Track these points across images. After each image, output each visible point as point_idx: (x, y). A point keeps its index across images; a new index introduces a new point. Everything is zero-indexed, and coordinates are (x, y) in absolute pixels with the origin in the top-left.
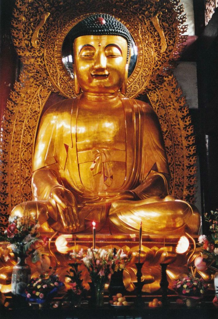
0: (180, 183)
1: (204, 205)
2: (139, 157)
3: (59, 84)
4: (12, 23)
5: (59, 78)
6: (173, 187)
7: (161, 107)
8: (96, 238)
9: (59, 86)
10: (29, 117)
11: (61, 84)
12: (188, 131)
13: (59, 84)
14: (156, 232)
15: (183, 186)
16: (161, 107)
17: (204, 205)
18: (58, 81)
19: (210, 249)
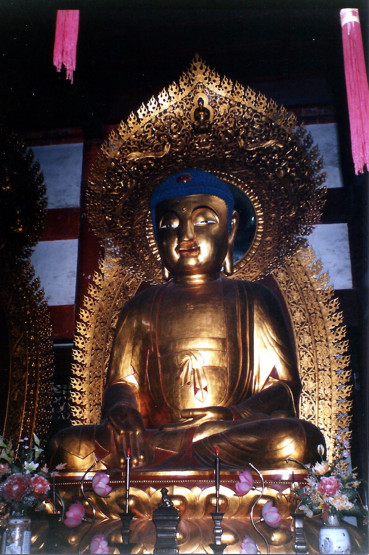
0: (327, 395)
1: (92, 183)
2: (248, 312)
3: (251, 275)
4: (160, 95)
5: (243, 275)
6: (315, 402)
7: (307, 332)
8: (331, 127)
9: (254, 273)
10: (286, 292)
11: (252, 272)
12: (337, 335)
13: (251, 275)
14: (265, 329)
15: (330, 400)
16: (307, 332)
17: (92, 183)
18: (246, 275)
19: (179, 146)
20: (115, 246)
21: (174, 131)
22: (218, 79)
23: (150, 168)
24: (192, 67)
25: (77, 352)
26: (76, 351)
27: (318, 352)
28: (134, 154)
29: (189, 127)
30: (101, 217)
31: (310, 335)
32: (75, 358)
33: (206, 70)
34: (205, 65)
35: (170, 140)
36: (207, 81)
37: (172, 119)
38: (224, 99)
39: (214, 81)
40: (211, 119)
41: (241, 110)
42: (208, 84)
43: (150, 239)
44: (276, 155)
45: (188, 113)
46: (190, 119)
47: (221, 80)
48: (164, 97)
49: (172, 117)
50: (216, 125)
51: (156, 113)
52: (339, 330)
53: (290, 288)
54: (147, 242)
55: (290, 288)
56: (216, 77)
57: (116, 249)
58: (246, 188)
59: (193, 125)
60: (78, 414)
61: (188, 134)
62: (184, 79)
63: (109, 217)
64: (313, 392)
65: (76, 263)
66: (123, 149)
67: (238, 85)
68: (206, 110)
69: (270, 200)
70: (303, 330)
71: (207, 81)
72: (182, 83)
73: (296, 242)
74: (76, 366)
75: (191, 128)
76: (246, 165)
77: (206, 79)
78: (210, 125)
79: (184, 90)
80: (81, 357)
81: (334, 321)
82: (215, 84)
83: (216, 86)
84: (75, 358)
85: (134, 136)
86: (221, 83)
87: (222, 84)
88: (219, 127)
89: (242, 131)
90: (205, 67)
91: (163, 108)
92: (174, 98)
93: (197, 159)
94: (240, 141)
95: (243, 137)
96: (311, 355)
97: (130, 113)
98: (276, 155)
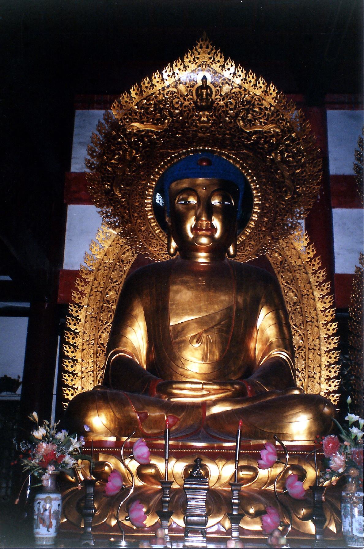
4: (175, 64)
13: (246, 253)
17: (167, 219)
20: (115, 217)
21: (176, 106)
22: (222, 60)
23: (151, 141)
24: (199, 46)
25: (68, 362)
26: (66, 375)
27: (309, 332)
28: (137, 125)
29: (190, 104)
30: (101, 187)
31: (302, 315)
32: (66, 397)
33: (212, 50)
34: (211, 45)
35: (171, 114)
36: (211, 61)
37: (175, 94)
38: (227, 80)
39: (218, 61)
40: (213, 97)
41: (243, 93)
42: (212, 64)
43: (151, 187)
44: (274, 139)
45: (190, 90)
46: (192, 95)
47: (225, 62)
48: (179, 67)
49: (175, 92)
50: (218, 104)
51: (159, 87)
52: (329, 312)
53: (283, 268)
54: (145, 214)
55: (283, 268)
56: (221, 57)
57: (115, 220)
58: (253, 181)
59: (195, 103)
60: (71, 339)
61: (189, 110)
62: (189, 56)
63: (108, 185)
64: (303, 370)
65: (68, 214)
66: (125, 119)
67: (240, 68)
68: (207, 87)
69: (268, 182)
70: (295, 310)
71: (211, 61)
72: (186, 60)
73: (290, 225)
74: (67, 376)
75: (193, 105)
76: (246, 147)
77: (210, 58)
78: (213, 102)
79: (188, 67)
80: (73, 352)
81: (325, 303)
82: (218, 64)
83: (220, 67)
84: (66, 397)
85: (136, 107)
86: (224, 64)
87: (226, 65)
88: (220, 106)
89: (242, 112)
90: (210, 47)
91: (167, 83)
92: (178, 74)
93: (201, 135)
94: (239, 122)
95: (243, 119)
96: (302, 334)
97: (145, 77)
98: (274, 139)
